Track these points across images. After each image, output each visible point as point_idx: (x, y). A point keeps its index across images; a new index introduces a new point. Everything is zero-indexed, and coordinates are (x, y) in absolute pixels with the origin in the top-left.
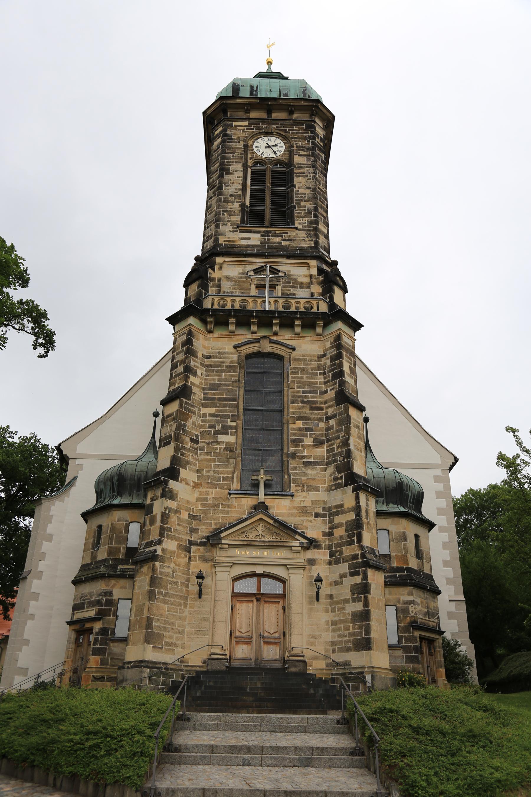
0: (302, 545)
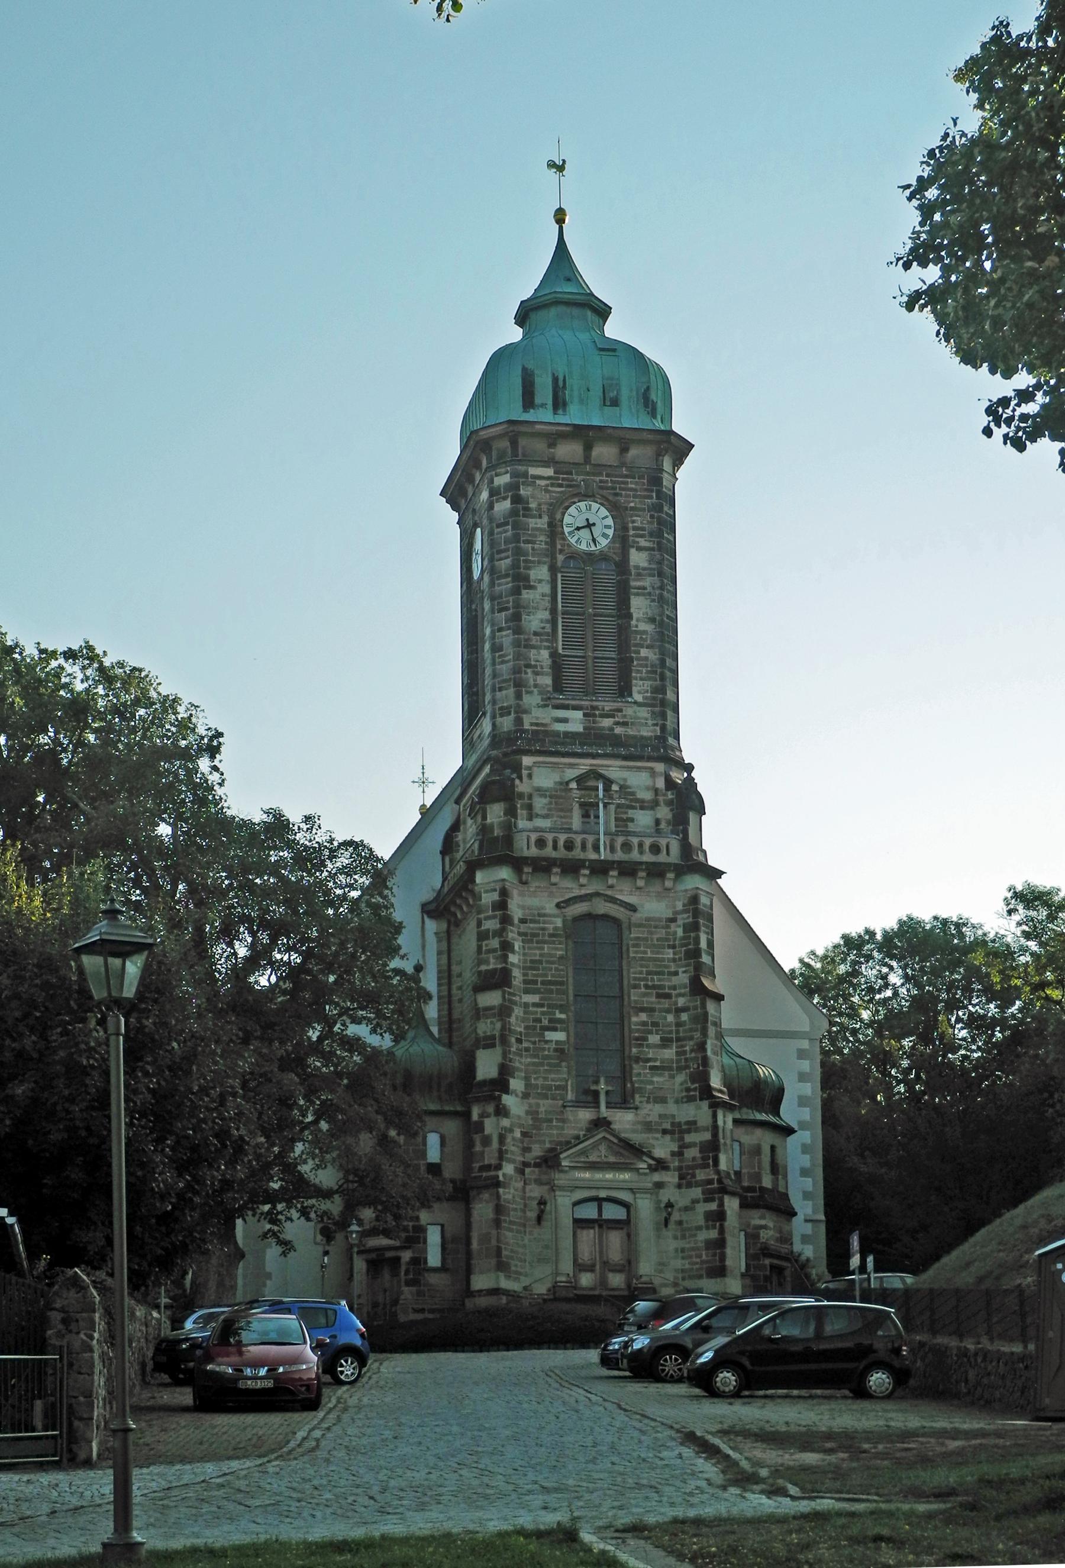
0: (650, 1167)
